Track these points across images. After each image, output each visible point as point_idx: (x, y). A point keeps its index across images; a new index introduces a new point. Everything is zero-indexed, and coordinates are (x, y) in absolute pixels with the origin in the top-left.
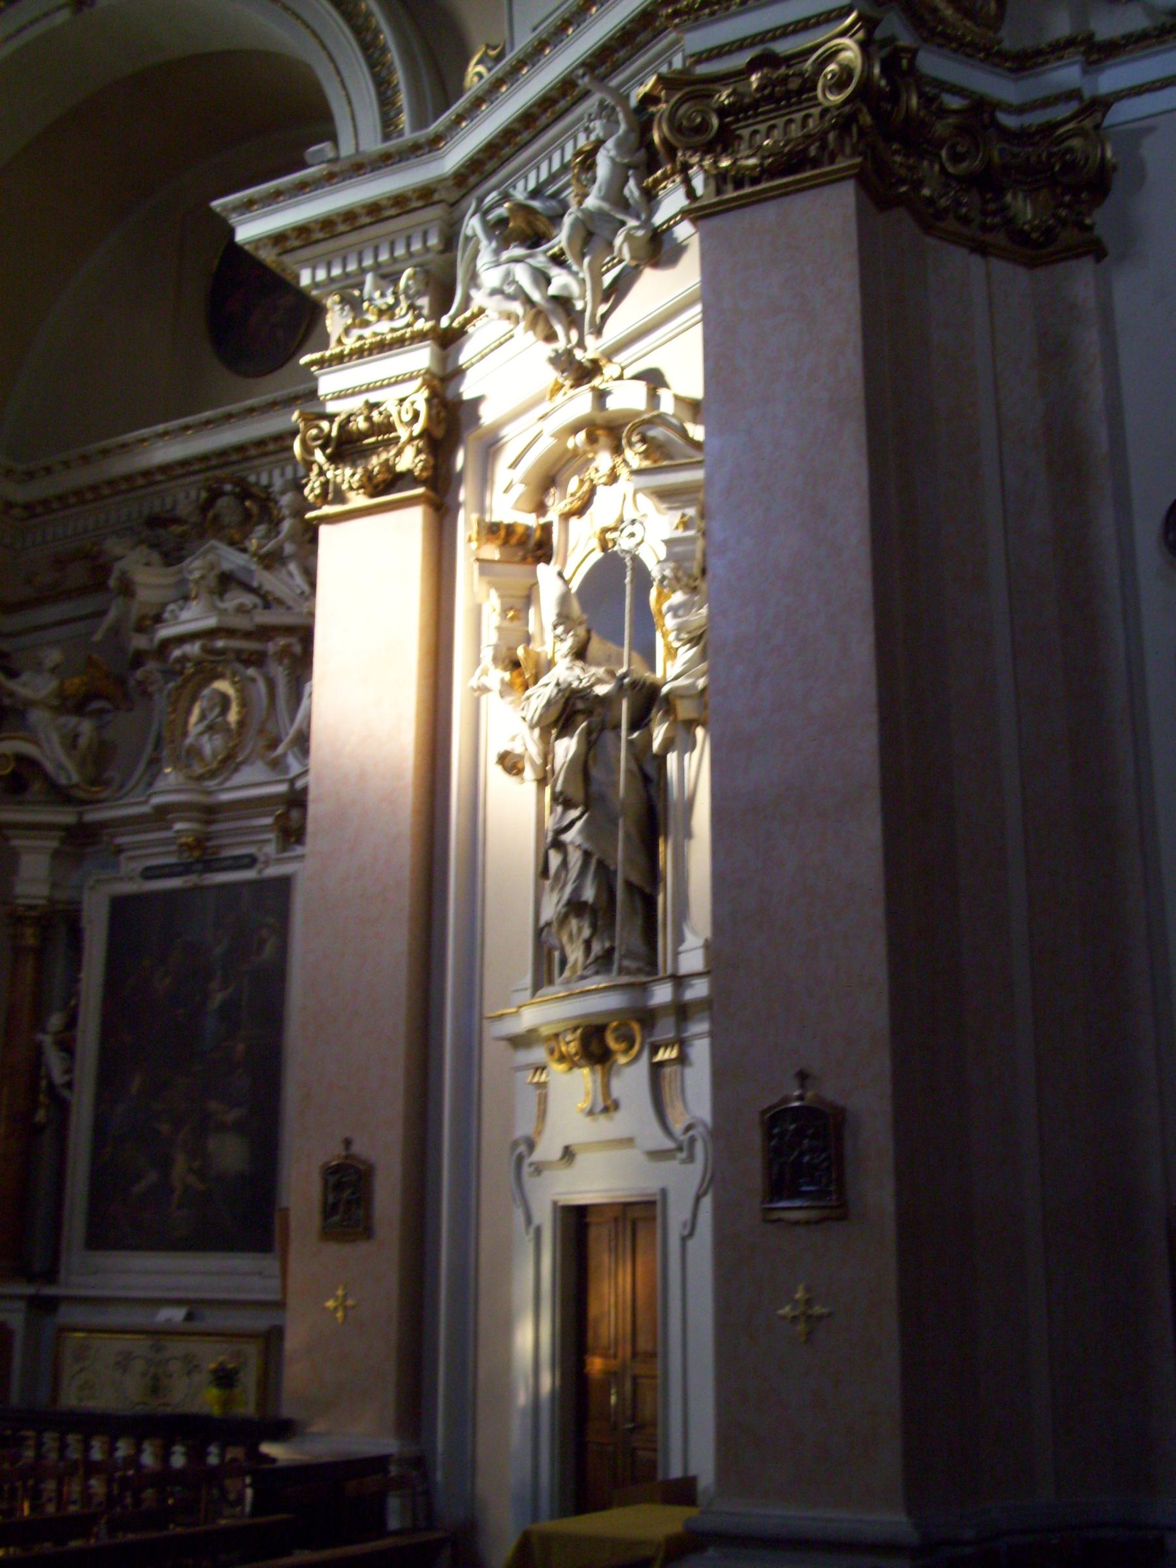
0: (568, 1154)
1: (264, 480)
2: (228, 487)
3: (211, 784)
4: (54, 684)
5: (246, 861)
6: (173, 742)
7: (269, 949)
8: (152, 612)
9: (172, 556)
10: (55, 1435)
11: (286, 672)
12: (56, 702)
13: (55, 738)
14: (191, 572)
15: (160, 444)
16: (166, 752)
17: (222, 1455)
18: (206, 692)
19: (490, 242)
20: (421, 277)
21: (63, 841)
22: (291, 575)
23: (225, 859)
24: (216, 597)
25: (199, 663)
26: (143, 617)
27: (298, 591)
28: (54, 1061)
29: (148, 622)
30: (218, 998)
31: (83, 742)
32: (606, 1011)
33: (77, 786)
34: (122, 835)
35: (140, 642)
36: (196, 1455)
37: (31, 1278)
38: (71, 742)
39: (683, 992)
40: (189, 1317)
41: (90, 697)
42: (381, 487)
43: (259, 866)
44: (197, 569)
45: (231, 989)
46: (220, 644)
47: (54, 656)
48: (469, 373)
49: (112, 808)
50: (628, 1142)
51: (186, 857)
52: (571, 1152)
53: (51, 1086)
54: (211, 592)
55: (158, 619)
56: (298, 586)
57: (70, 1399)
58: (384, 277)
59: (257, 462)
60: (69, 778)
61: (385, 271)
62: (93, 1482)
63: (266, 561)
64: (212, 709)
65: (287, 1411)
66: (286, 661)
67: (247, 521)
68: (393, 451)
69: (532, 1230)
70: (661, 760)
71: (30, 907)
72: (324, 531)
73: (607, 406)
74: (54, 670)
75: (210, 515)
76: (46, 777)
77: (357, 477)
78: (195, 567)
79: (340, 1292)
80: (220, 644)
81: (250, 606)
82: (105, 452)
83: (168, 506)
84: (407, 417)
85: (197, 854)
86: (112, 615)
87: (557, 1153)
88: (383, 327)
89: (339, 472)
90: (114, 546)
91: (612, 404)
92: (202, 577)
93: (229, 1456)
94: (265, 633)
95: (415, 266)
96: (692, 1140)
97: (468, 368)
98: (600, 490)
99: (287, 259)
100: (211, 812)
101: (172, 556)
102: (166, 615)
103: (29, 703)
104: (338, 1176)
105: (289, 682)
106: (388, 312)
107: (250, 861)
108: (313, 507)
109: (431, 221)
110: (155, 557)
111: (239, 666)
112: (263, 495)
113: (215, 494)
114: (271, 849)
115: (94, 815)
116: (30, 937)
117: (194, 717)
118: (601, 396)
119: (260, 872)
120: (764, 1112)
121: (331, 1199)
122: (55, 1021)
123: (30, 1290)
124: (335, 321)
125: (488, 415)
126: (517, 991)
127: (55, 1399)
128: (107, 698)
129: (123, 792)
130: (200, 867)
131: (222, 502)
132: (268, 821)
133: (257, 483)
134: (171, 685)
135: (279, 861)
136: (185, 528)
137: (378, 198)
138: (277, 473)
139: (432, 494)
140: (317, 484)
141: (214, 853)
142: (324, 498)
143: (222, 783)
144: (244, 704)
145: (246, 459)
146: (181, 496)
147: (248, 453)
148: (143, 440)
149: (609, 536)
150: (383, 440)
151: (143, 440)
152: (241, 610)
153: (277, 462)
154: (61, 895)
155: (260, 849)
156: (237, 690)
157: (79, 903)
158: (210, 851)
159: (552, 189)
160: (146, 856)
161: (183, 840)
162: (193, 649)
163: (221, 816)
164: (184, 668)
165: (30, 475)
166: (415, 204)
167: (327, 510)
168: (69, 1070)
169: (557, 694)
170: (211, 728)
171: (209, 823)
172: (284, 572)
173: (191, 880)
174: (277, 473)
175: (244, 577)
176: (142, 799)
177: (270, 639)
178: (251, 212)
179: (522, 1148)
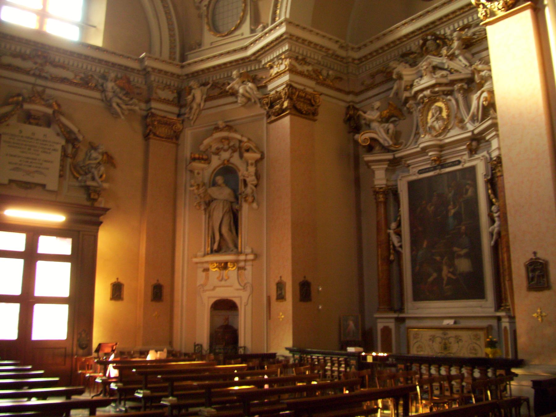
1: (442, 32)
2: (429, 37)
3: (441, 138)
5: (457, 163)
6: (423, 126)
7: (470, 193)
8: (409, 84)
9: (413, 64)
10: (418, 365)
11: (462, 96)
12: (380, 120)
13: (382, 130)
14: (422, 67)
16: (421, 130)
17: (494, 373)
18: (433, 107)
21: (389, 165)
22: (460, 61)
24: (433, 74)
25: (429, 97)
26: (407, 86)
27: (464, 66)
28: (394, 239)
29: (408, 88)
30: (453, 211)
31: (391, 131)
33: (391, 146)
34: (409, 160)
35: (406, 94)
36: (484, 373)
37: (395, 311)
38: (387, 132)
40: (455, 323)
42: (511, 6)
43: (462, 164)
44: (425, 65)
45: (457, 207)
46: (437, 89)
47: (377, 104)
49: (404, 151)
51: (434, 164)
53: (394, 247)
54: (431, 72)
55: (412, 86)
56: (464, 64)
57: (414, 352)
59: (439, 27)
60: (388, 143)
62: (453, 383)
63: (451, 58)
64: (436, 113)
65: (520, 356)
66: (461, 92)
67: (438, 47)
71: (381, 188)
72: (488, 28)
74: (378, 109)
75: (424, 48)
76: (380, 144)
78: (423, 65)
79: (539, 311)
80: (437, 89)
82: (384, 35)
83: (408, 49)
85: (438, 163)
86: (395, 87)
89: (492, 4)
90: (392, 64)
92: (427, 68)
93: (498, 373)
94: (452, 83)
100: (441, 147)
101: (413, 64)
102: (415, 83)
103: (371, 121)
104: (533, 266)
105: (463, 99)
107: (459, 162)
108: (482, 21)
110: (407, 65)
111: (444, 97)
112: (443, 37)
113: (425, 41)
114: (466, 157)
115: (398, 155)
116: (381, 198)
117: (430, 115)
119: (463, 166)
121: (530, 275)
122: (393, 225)
123: (396, 315)
127: (408, 352)
129: (407, 146)
130: (440, 167)
131: (428, 43)
132: (464, 147)
133: (440, 34)
134: (419, 107)
135: (469, 161)
136: (415, 55)
138: (447, 29)
139: (532, 4)
140: (483, 11)
141: (444, 162)
142: (486, 16)
144: (448, 108)
146: (412, 45)
148: (398, 28)
151: (398, 28)
152: (443, 76)
154: (389, 184)
155: (462, 158)
156: (445, 104)
157: (396, 185)
158: (442, 161)
161: (433, 158)
162: (427, 93)
163: (445, 148)
164: (424, 101)
165: (359, 48)
167: (488, 20)
168: (400, 241)
171: (441, 151)
172: (457, 60)
173: (437, 172)
174: (447, 29)
175: (441, 66)
176: (416, 146)
177: (454, 85)
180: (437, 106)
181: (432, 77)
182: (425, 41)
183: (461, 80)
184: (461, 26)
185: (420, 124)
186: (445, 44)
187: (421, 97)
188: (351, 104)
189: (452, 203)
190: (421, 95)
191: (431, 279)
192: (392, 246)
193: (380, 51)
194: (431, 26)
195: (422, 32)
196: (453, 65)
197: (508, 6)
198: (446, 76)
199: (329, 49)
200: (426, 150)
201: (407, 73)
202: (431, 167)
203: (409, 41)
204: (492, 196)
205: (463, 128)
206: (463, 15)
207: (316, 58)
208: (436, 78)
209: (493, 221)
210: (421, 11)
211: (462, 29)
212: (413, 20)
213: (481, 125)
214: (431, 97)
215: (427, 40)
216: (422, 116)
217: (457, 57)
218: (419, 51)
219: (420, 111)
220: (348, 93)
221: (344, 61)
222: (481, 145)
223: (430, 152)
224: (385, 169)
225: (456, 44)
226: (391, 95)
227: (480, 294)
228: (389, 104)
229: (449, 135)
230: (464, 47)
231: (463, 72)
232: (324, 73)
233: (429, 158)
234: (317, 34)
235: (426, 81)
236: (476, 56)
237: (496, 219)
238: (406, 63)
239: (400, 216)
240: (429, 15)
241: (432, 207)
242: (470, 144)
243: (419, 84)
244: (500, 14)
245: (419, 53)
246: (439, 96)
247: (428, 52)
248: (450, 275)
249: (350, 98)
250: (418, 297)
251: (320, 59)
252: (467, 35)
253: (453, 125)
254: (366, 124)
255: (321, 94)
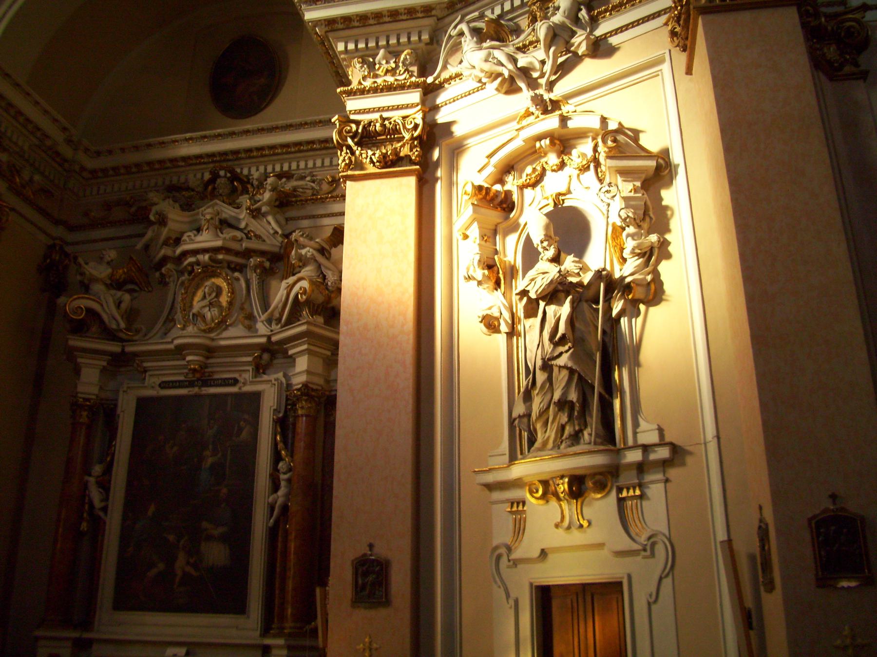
0: (544, 553)
1: (245, 172)
2: (222, 173)
3: (212, 335)
4: (110, 270)
7: (244, 435)
11: (258, 277)
12: (109, 282)
13: (111, 301)
15: (186, 144)
16: (179, 316)
18: (208, 283)
19: (473, 38)
20: (414, 55)
22: (269, 223)
23: (218, 379)
25: (205, 266)
28: (95, 495)
30: (210, 460)
31: (123, 306)
32: (588, 466)
33: (121, 330)
35: (165, 251)
38: (118, 305)
39: (648, 455)
41: (125, 282)
44: (209, 213)
45: (220, 455)
46: (220, 257)
47: (112, 254)
48: (442, 109)
50: (601, 546)
52: (545, 552)
55: (178, 241)
58: (390, 53)
59: (242, 162)
60: (118, 325)
61: (391, 49)
68: (400, 144)
69: (512, 602)
70: (617, 320)
71: (88, 400)
73: (568, 126)
76: (102, 321)
77: (377, 155)
78: (207, 212)
80: (220, 257)
81: (240, 238)
82: (149, 145)
84: (410, 127)
85: (198, 375)
86: (150, 234)
87: (536, 553)
88: (390, 79)
90: (153, 196)
91: (571, 124)
92: (212, 218)
94: (248, 253)
95: (411, 49)
96: (653, 545)
97: (442, 106)
98: (549, 173)
99: (331, 36)
100: (210, 351)
101: (187, 206)
102: (185, 237)
106: (393, 72)
107: (235, 382)
109: (425, 26)
111: (229, 272)
113: (215, 176)
114: (248, 376)
115: (130, 349)
118: (564, 120)
119: (240, 388)
120: (810, 520)
122: (98, 469)
123: (75, 634)
124: (356, 74)
125: (458, 131)
126: (493, 456)
128: (136, 284)
129: (147, 337)
132: (250, 359)
135: (252, 383)
137: (398, 7)
141: (209, 376)
142: (348, 166)
143: (218, 335)
145: (237, 159)
147: (240, 156)
148: (176, 141)
149: (561, 198)
150: (397, 138)
151: (176, 141)
152: (234, 239)
153: (271, 161)
156: (228, 284)
157: (117, 400)
159: (510, 16)
160: (164, 375)
164: (193, 270)
165: (98, 154)
166: (420, 15)
167: (350, 173)
169: (559, 277)
170: (211, 304)
171: (207, 358)
173: (196, 390)
175: (233, 222)
178: (316, 4)
179: (503, 551)
180: (214, 283)
181: (218, 236)
182: (215, 176)
183: (262, 253)
184: (277, 172)
185: (179, 306)
186: (245, 191)
187: (190, 262)
188: (57, 242)
189: (211, 447)
190: (191, 259)
191: (153, 572)
192: (87, 507)
193: (134, 170)
194: (230, 157)
195: (213, 162)
196: (255, 226)
197: (386, 163)
198: (241, 240)
199: (47, 137)
200: (183, 351)
201: (176, 217)
202: (186, 381)
203: (188, 168)
204: (280, 446)
205: (251, 328)
206: (285, 156)
207: (20, 143)
208: (225, 239)
209: (276, 488)
210: (222, 128)
211: (279, 176)
212: (205, 137)
213: (322, 327)
214: (209, 266)
215: (219, 176)
216: (186, 293)
217: (264, 215)
218: (200, 189)
219: (183, 283)
220: (57, 222)
221: (66, 165)
222: (275, 362)
223: (190, 354)
224: (101, 367)
225: (267, 195)
226: (139, 246)
227: (240, 608)
228: (131, 258)
229: (225, 334)
230: (277, 203)
231: (268, 241)
232: (26, 174)
233: (185, 365)
234: (37, 103)
235: (206, 239)
236: (290, 222)
237: (283, 483)
238: (175, 201)
239: (113, 455)
240: (304, 128)
241: (175, 449)
242: (260, 357)
243: (192, 241)
244: (371, 169)
245: (198, 192)
246: (222, 268)
247: (214, 195)
248: (189, 569)
249: (58, 231)
250: (122, 603)
251: (26, 148)
252: (283, 187)
253: (235, 320)
254: (82, 283)
255: (13, 209)
